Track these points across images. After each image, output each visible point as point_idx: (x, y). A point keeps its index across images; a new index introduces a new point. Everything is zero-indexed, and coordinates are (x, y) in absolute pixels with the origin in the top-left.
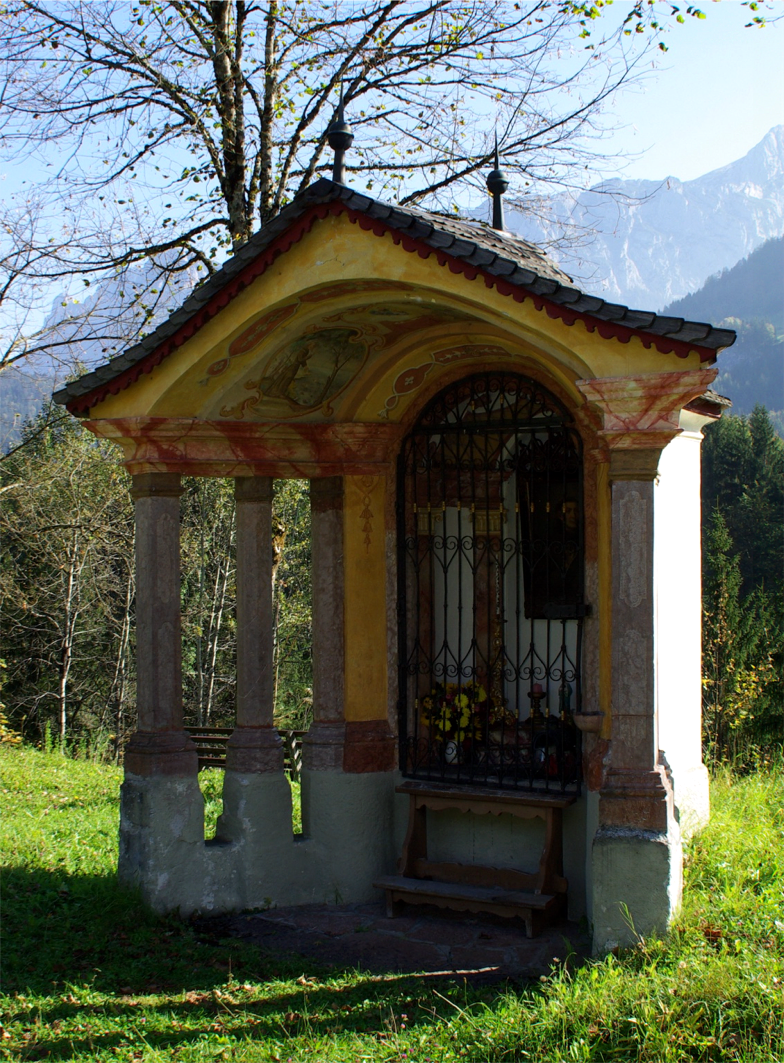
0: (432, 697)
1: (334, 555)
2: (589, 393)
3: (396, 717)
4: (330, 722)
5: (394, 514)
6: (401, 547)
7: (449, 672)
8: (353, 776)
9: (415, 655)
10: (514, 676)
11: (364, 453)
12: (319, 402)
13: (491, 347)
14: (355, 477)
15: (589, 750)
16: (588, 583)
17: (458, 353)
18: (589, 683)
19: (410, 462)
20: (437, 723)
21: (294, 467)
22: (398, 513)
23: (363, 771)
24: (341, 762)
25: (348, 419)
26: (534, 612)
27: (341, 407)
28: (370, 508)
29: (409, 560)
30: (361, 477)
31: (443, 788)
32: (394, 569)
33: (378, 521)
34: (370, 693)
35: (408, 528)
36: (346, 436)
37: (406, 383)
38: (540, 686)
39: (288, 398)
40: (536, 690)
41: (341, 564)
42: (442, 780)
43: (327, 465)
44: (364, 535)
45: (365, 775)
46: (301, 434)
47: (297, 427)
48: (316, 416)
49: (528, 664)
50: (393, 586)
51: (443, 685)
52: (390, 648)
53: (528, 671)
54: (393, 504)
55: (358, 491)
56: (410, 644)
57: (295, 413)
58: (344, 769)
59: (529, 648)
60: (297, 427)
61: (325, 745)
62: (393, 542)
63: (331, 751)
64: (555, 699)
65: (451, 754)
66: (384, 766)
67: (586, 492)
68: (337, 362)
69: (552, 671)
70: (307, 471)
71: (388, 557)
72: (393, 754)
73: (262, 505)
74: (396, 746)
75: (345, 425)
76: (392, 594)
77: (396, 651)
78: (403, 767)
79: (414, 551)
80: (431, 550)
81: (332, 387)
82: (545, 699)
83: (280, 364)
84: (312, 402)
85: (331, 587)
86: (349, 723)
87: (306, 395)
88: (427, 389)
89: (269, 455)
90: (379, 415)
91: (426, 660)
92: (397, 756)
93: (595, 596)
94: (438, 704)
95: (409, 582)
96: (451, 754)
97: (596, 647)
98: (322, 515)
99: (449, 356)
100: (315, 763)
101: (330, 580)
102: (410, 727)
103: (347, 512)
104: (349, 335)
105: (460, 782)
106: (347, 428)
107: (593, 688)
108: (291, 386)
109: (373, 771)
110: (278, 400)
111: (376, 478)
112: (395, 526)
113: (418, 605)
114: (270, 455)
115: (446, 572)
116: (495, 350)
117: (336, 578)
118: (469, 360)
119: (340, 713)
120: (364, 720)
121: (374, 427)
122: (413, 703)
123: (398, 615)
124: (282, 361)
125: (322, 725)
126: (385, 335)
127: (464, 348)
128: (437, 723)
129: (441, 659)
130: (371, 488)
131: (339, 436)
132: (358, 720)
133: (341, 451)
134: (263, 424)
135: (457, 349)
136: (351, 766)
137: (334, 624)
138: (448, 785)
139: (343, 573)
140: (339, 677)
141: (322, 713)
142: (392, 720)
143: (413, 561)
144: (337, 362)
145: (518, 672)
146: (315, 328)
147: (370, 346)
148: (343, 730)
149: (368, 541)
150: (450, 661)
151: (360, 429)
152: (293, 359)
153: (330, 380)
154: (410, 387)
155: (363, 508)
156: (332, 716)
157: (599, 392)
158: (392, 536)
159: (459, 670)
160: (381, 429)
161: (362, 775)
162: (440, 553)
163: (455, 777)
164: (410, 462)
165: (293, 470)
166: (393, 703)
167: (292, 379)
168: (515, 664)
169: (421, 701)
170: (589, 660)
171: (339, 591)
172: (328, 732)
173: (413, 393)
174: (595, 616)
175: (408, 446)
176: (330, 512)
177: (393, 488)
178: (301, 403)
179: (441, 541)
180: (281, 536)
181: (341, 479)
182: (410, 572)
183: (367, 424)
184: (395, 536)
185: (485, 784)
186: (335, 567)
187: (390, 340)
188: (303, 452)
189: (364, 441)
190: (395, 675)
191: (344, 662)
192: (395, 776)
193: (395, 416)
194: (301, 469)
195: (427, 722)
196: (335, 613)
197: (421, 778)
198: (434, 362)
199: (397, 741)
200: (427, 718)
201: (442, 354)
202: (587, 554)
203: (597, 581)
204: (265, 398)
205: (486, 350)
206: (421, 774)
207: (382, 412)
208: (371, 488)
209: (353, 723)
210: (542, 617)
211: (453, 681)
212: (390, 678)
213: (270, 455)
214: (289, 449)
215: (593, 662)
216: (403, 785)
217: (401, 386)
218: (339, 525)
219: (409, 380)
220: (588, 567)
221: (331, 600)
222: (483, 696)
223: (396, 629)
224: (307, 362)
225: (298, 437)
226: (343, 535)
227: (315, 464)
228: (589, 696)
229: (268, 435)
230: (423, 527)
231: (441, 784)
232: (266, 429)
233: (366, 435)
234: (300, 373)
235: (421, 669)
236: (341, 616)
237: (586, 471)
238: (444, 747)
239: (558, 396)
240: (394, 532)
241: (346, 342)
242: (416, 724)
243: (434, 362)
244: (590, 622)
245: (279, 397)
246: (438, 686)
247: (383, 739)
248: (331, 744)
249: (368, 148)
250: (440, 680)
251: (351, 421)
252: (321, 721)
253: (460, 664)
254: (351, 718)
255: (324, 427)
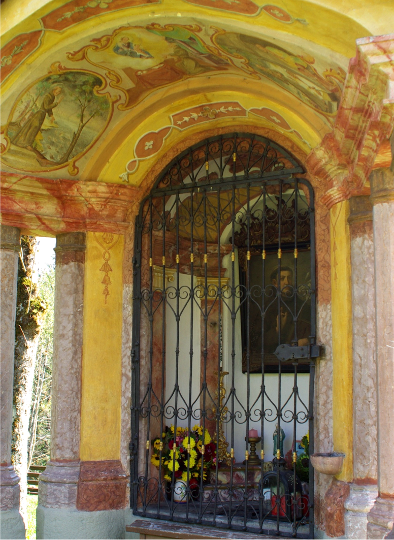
0: (163, 439)
1: (74, 303)
2: (373, 54)
3: (129, 457)
4: (65, 461)
5: (132, 269)
6: (137, 299)
7: (179, 415)
8: (86, 514)
9: (147, 401)
10: (244, 418)
11: (105, 213)
12: (65, 159)
13: (226, 104)
14: (97, 234)
15: (323, 493)
16: (320, 324)
17: (195, 115)
18: (322, 424)
19: (148, 222)
20: (166, 463)
21: (40, 219)
22: (135, 268)
23: (96, 509)
24: (74, 500)
25: (92, 179)
26: (250, 368)
27: (85, 166)
28: (109, 262)
29: (144, 311)
30: (102, 234)
31: (173, 528)
32: (130, 320)
33: (116, 275)
34: (106, 436)
35: (144, 281)
36: (89, 194)
37: (146, 148)
38: (256, 431)
39: (35, 150)
40: (252, 434)
41: (81, 313)
42: (171, 519)
43: (71, 221)
44: (104, 286)
45: (97, 513)
46: (48, 189)
47: (41, 180)
48: (63, 173)
49: (258, 406)
50: (128, 335)
51: (173, 429)
52: (124, 392)
53: (258, 413)
54: (131, 260)
55: (99, 246)
56: (143, 389)
57: (44, 168)
58: (77, 508)
59: (259, 390)
60: (41, 180)
61: (60, 483)
62: (130, 294)
63: (64, 489)
64: (269, 442)
65: (180, 490)
66: (115, 504)
67: (318, 237)
68: (82, 117)
69: (283, 412)
70: (52, 226)
71: (124, 309)
72: (124, 493)
73: (9, 253)
74: (128, 485)
75: (89, 183)
76: (127, 342)
77: (130, 395)
78: (134, 505)
79: (148, 302)
80: (164, 300)
81: (77, 145)
82: (260, 442)
83: (26, 107)
84: (59, 159)
85: (71, 333)
86: (83, 463)
87: (53, 150)
88: (164, 156)
89: (17, 207)
90: (121, 178)
91: (157, 405)
92: (128, 495)
93: (328, 337)
94: (167, 446)
95: (144, 332)
96: (180, 490)
97: (329, 388)
98: (65, 266)
99: (186, 119)
100: (50, 501)
101: (70, 326)
102: (142, 468)
103: (88, 265)
104: (94, 85)
105: (188, 522)
106: (91, 186)
107: (326, 429)
108: (38, 137)
109: (105, 509)
110: (25, 151)
111: (116, 237)
112: (131, 279)
113: (151, 353)
114: (18, 207)
115: (178, 320)
116: (230, 109)
117: (76, 325)
118: (205, 125)
119: (75, 453)
120: (98, 460)
121: (117, 188)
122: (145, 444)
123: (133, 362)
124: (28, 104)
125: (58, 464)
126: (128, 91)
127: (201, 108)
128: (166, 463)
129: (172, 403)
130: (111, 245)
131: (83, 194)
132: (92, 460)
133: (84, 211)
134: (11, 175)
135: (195, 110)
136: (84, 504)
137: (72, 368)
138: (177, 524)
139: (82, 320)
140: (75, 418)
141: (58, 452)
142: (125, 460)
143: (148, 310)
144: (82, 117)
145: (248, 415)
146: (60, 67)
147: (114, 103)
148: (78, 469)
149: (106, 292)
150: (181, 404)
151: (102, 189)
152: (39, 104)
153: (76, 137)
154: (149, 152)
155: (104, 262)
156: (68, 455)
157: (385, 52)
158: (129, 289)
159: (190, 413)
160: (122, 191)
161: (94, 512)
162: (173, 302)
163: (184, 516)
164: (148, 222)
165: (39, 223)
166: (126, 444)
167: (39, 129)
168: (246, 409)
169: (152, 443)
170: (321, 402)
171: (78, 337)
172: (63, 471)
173: (151, 159)
174: (328, 357)
175: (146, 208)
176: (72, 264)
177: (131, 245)
178: (48, 157)
179: (174, 292)
180: (43, 312)
181: (84, 235)
182: (145, 323)
183: (109, 185)
184: (131, 289)
185: (214, 525)
186: (75, 315)
187: (133, 97)
188: (49, 208)
189: (107, 201)
190: (128, 418)
191: (81, 405)
192: (126, 515)
193: (135, 180)
194: (47, 222)
195: (157, 463)
196: (73, 358)
197: (151, 516)
198: (172, 126)
199: (129, 480)
200: (157, 458)
201: (180, 116)
202: (319, 296)
203: (330, 323)
204: (13, 147)
205: (222, 109)
206: (151, 512)
207: (124, 175)
208: (111, 245)
209: (89, 462)
210: (258, 371)
211: (182, 424)
212: (123, 421)
213: (18, 207)
214: (36, 204)
215: (326, 403)
216: (133, 524)
217: (141, 151)
218: (81, 273)
219: (149, 145)
220: (320, 309)
221: (70, 345)
222: (208, 440)
223: (130, 374)
224: (54, 110)
225: (45, 192)
226: (83, 286)
227: (60, 219)
228: (322, 437)
229: (16, 187)
230: (157, 284)
231: (171, 524)
232: (14, 180)
233: (107, 195)
234: (47, 124)
235: (153, 412)
236: (79, 361)
237: (318, 217)
238: (170, 486)
239: (290, 150)
240: (131, 286)
241: (91, 93)
242: (147, 464)
243: (172, 126)
244: (323, 363)
245: (26, 148)
246: (167, 429)
247: (116, 478)
248: (65, 483)
249: (122, 365)
250: (170, 423)
251: (95, 180)
252: (57, 460)
253: (190, 407)
254: (85, 458)
255: (70, 183)
